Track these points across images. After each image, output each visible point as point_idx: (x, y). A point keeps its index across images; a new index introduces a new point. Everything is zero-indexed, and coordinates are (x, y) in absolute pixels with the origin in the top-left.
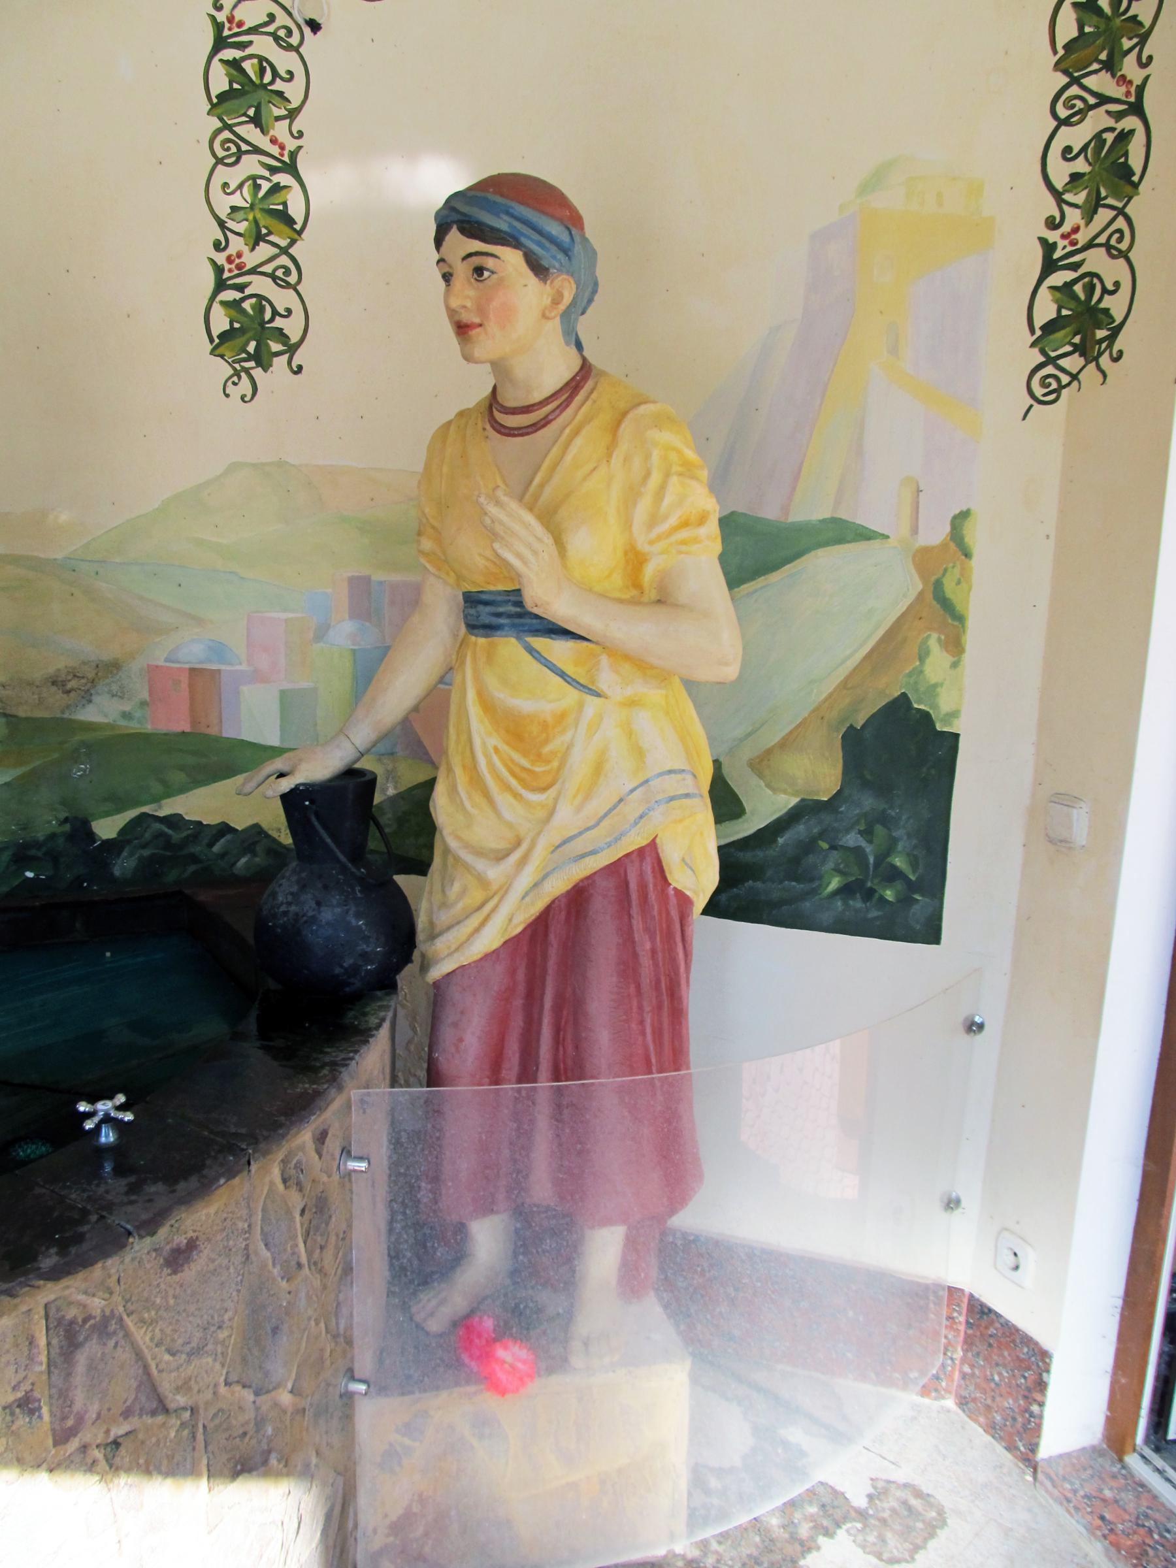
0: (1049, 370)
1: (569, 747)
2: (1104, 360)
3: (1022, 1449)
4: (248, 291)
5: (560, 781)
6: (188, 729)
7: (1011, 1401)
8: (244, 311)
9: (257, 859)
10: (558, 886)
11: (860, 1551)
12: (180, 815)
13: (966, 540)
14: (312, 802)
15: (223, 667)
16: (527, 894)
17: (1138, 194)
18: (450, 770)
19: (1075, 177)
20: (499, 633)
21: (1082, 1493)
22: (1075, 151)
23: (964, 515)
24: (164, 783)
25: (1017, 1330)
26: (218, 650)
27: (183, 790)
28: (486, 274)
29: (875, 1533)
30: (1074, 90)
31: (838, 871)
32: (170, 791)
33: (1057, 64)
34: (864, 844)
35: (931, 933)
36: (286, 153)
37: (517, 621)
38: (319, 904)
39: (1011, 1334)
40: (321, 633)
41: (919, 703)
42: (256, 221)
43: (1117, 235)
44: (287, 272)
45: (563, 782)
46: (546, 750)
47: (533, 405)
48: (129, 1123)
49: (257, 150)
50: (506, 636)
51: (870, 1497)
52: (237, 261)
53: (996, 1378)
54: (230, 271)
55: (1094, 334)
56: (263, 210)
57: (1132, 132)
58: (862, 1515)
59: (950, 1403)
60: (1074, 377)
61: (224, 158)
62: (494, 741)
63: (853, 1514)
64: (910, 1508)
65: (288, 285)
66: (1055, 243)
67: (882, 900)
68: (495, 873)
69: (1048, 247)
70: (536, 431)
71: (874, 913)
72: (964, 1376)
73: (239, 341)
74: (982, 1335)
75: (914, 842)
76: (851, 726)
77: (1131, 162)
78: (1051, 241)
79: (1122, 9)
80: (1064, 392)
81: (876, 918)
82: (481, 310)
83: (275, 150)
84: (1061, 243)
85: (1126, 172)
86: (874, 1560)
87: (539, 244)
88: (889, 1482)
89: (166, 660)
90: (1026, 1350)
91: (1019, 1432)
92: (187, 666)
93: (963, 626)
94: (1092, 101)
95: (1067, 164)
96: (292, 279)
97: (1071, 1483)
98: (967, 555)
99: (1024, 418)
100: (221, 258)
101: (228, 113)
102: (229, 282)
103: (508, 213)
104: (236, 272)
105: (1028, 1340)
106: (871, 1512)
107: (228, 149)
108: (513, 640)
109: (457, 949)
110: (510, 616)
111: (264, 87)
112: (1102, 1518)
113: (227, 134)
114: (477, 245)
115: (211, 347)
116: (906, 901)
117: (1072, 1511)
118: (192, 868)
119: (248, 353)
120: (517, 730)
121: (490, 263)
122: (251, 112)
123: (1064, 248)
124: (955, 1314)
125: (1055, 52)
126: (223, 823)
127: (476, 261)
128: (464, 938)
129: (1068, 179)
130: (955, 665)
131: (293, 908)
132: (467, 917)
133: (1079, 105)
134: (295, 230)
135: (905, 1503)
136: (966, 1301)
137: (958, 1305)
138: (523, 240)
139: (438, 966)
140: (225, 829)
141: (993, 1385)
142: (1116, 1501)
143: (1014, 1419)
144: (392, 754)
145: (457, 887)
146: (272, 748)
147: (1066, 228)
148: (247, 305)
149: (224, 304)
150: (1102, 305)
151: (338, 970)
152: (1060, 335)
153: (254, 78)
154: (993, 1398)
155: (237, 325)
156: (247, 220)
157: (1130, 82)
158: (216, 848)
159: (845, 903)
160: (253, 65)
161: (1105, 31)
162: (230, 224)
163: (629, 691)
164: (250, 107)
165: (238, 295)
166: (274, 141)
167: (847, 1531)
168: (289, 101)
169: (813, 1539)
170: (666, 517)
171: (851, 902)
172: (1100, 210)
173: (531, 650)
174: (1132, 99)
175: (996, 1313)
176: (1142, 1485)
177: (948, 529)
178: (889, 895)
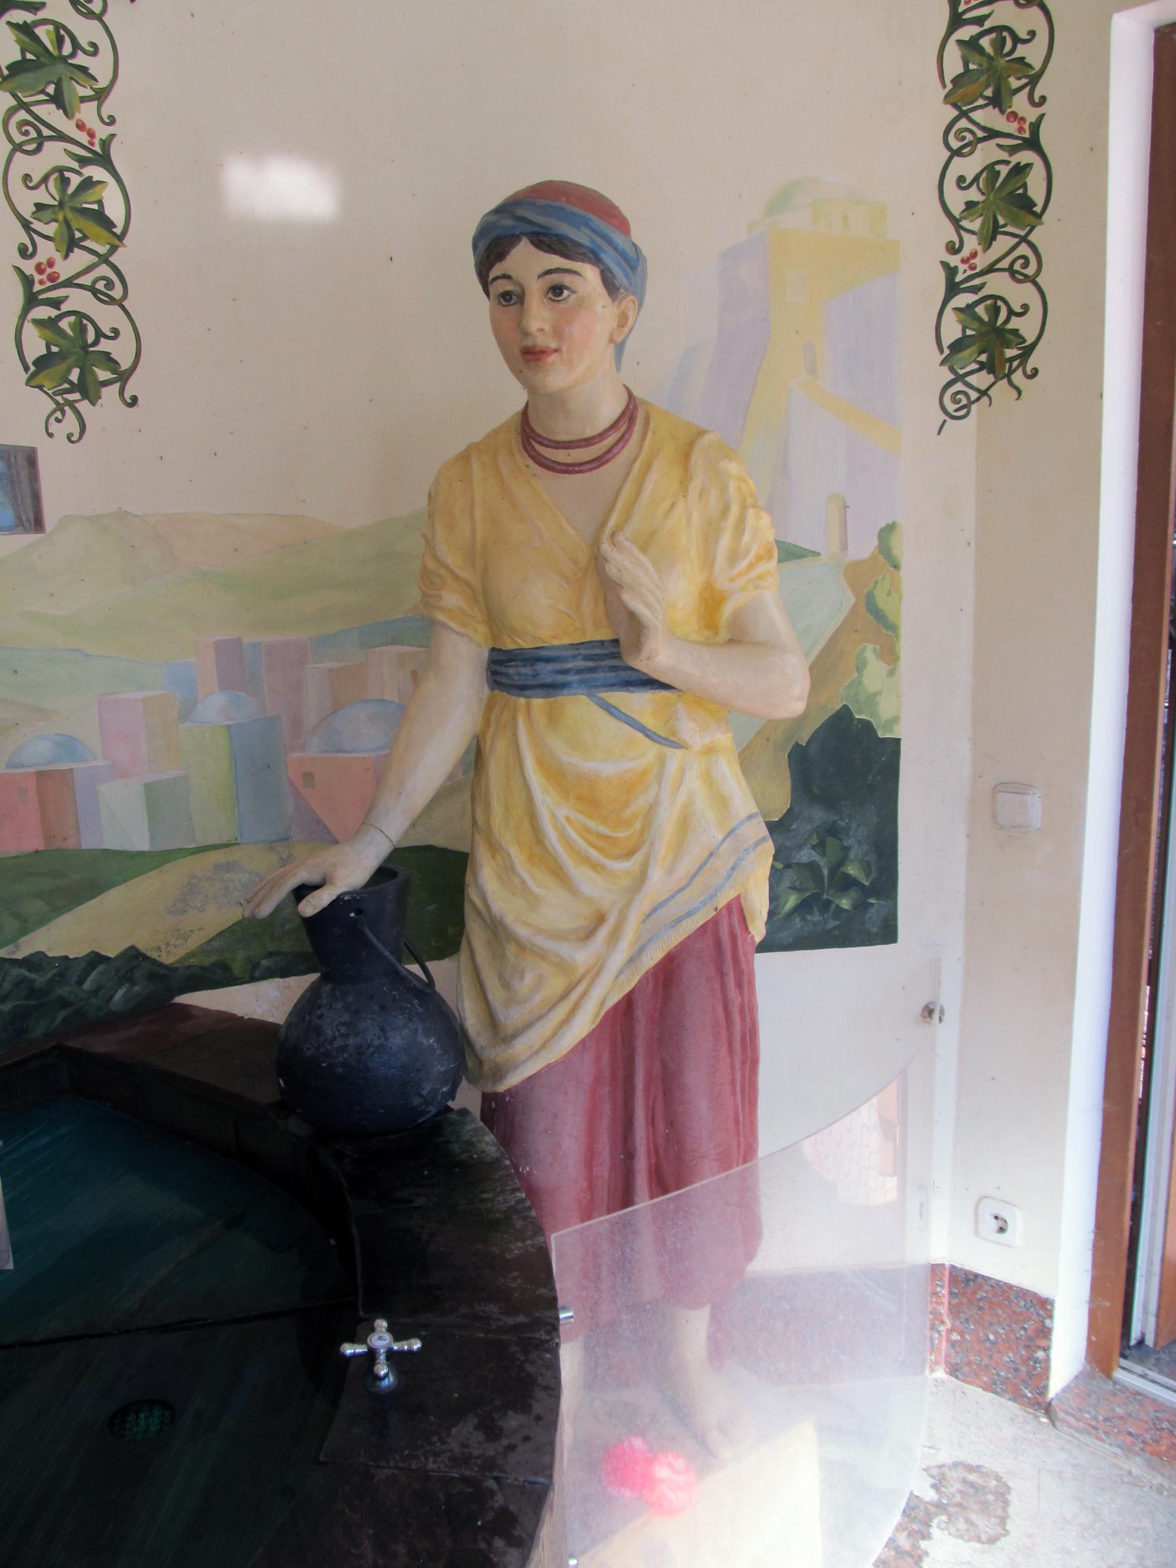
0: (959, 386)
1: (652, 808)
2: (1018, 377)
3: (1029, 1395)
4: (65, 308)
5: (647, 843)
6: (41, 847)
7: (1011, 1355)
8: (61, 333)
9: (137, 988)
10: (653, 957)
11: (960, 1541)
12: (43, 953)
13: (894, 552)
14: (359, 912)
15: (75, 765)
16: (621, 972)
17: (1042, 224)
18: (495, 848)
19: (970, 205)
20: (565, 691)
21: (1101, 1418)
22: (969, 181)
23: (890, 528)
24: (17, 916)
25: (1010, 1287)
26: (68, 746)
27: (43, 921)
28: (566, 293)
29: (961, 1520)
30: (963, 123)
31: (793, 888)
32: (27, 926)
33: (946, 97)
34: (817, 858)
35: (887, 933)
36: (97, 141)
37: (587, 676)
38: (382, 1030)
39: (1004, 1292)
40: (186, 713)
41: (860, 713)
42: (67, 223)
43: (1021, 261)
44: (110, 285)
45: (652, 844)
46: (627, 813)
47: (593, 437)
48: (420, 1351)
49: (61, 137)
50: (574, 694)
51: (934, 1486)
52: (49, 271)
53: (992, 1337)
54: (41, 282)
55: (1002, 353)
56: (75, 210)
57: (1029, 166)
58: (940, 1507)
59: (941, 1373)
60: (983, 393)
61: (22, 144)
62: (565, 811)
63: (933, 1509)
64: (972, 1485)
65: (112, 301)
66: (956, 267)
67: (839, 910)
68: (583, 957)
69: (951, 272)
70: (599, 466)
71: (832, 923)
72: (953, 1344)
73: (61, 368)
74: (969, 1301)
75: (865, 847)
76: (797, 743)
77: (1030, 193)
78: (952, 265)
79: (1006, 50)
80: (974, 407)
81: (835, 928)
82: (558, 332)
83: (83, 138)
84: (962, 267)
85: (1026, 204)
86: (978, 1545)
87: (619, 266)
88: (940, 1467)
89: (8, 767)
90: (1022, 1303)
91: (1024, 1383)
92: (34, 770)
93: (897, 636)
94: (980, 134)
95: (961, 192)
96: (117, 293)
97: (1089, 1413)
98: (896, 566)
99: (939, 433)
100: (29, 267)
101: (22, 88)
102: (41, 297)
103: (587, 225)
104: (49, 284)
105: (1023, 1293)
106: (945, 1501)
107: (26, 133)
108: (583, 698)
109: (544, 1046)
110: (579, 671)
111: (64, 59)
112: (1130, 1434)
113: (22, 115)
114: (556, 261)
115: (25, 376)
116: (861, 906)
117: (1103, 1437)
118: (62, 1015)
119: (71, 383)
120: (586, 794)
121: (567, 279)
122: (51, 89)
123: (965, 271)
124: (938, 1289)
125: (944, 86)
126: (93, 952)
127: (555, 278)
128: (549, 1033)
129: (963, 207)
130: (891, 673)
131: (351, 1041)
132: (550, 1010)
133: (969, 137)
134: (115, 234)
135: (965, 1481)
136: (947, 1274)
137: (941, 1280)
138: (603, 256)
139: (519, 1071)
140: (95, 960)
141: (988, 1345)
142: (1130, 1415)
143: (1016, 1370)
144: (286, 839)
145: (529, 978)
146: (141, 854)
147: (965, 253)
148: (65, 324)
149: (38, 323)
150: (1009, 326)
151: (417, 1101)
152: (966, 353)
153: (50, 48)
154: (990, 1357)
155: (55, 349)
156: (56, 221)
157: (1023, 119)
158: (87, 985)
159: (803, 919)
160: (48, 32)
161: (988, 70)
162: (37, 225)
163: (707, 740)
164: (49, 83)
165: (53, 313)
166: (81, 126)
167: (939, 1527)
168: (96, 80)
169: (915, 1546)
170: (748, 552)
171: (809, 917)
172: (999, 237)
173: (608, 708)
174: (1027, 135)
175: (983, 1277)
176: (1139, 1394)
177: (876, 542)
178: (845, 903)
